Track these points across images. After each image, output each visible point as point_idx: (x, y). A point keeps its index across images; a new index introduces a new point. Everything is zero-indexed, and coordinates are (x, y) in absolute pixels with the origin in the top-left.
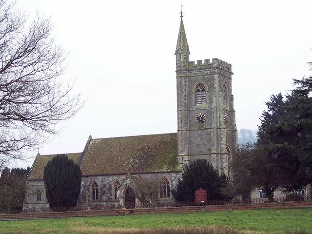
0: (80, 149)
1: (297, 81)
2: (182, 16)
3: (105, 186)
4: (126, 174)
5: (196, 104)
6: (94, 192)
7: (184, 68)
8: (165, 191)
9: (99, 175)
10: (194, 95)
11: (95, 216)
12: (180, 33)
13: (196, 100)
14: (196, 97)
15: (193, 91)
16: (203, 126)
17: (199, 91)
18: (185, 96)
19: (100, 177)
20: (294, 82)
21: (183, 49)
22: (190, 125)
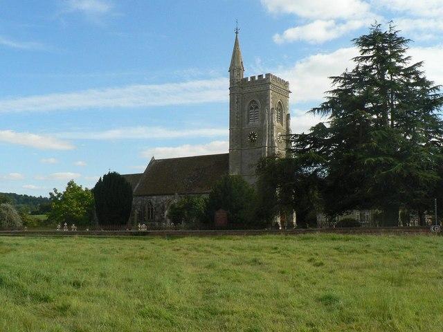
0: (140, 168)
1: (337, 79)
2: (237, 33)
3: (159, 205)
4: (173, 194)
5: (249, 122)
6: (149, 212)
7: (237, 85)
8: (149, 212)
9: (154, 195)
10: (246, 112)
11: (49, 233)
12: (235, 48)
13: (248, 118)
14: (248, 115)
15: (246, 107)
16: (254, 145)
17: (252, 108)
18: (238, 113)
19: (155, 197)
20: (333, 80)
21: (235, 68)
22: (242, 145)
